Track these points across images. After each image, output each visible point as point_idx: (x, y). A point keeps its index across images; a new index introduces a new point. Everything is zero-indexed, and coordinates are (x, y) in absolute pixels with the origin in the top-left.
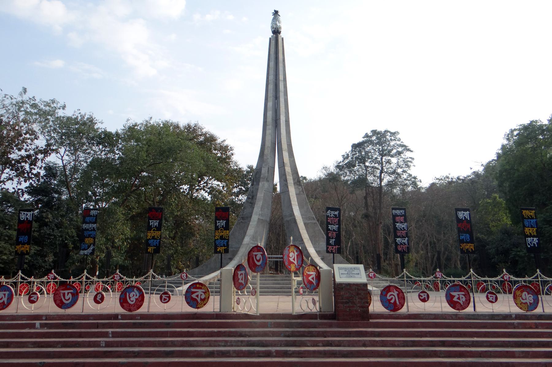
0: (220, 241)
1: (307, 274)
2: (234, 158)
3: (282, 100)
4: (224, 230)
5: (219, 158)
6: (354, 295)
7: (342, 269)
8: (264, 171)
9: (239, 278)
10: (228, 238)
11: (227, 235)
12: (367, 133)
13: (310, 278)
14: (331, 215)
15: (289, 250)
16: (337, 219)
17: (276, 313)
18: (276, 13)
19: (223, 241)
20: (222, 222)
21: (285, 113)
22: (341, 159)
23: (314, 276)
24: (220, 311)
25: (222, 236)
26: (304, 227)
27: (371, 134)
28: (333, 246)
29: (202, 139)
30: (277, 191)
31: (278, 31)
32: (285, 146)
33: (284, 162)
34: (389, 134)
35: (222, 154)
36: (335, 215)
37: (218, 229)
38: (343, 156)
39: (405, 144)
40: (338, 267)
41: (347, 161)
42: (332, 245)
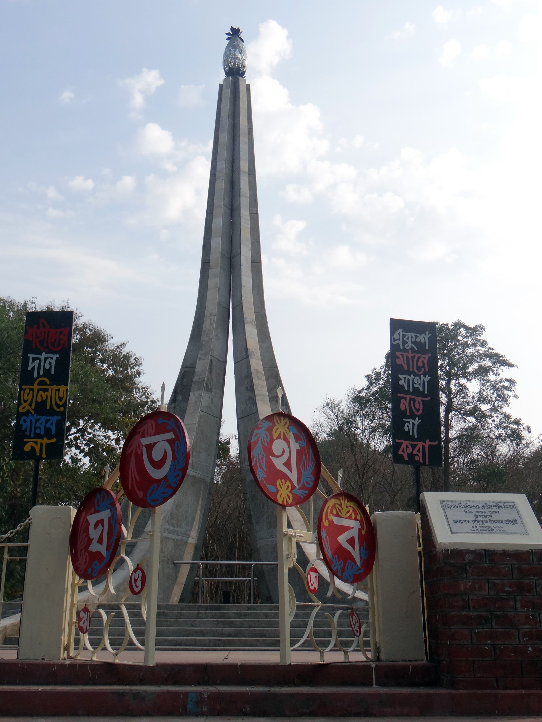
1: (331, 522)
2: (142, 381)
3: (245, 213)
4: (52, 384)
5: (110, 379)
6: (507, 592)
7: (454, 506)
9: (91, 537)
10: (62, 409)
13: (342, 539)
14: (404, 343)
15: (270, 430)
18: (235, 33)
19: (44, 418)
20: (46, 359)
21: (252, 243)
22: (365, 383)
23: (354, 533)
24: (18, 658)
25: (44, 402)
30: (229, 457)
31: (238, 69)
32: (249, 313)
33: (246, 349)
34: (463, 331)
35: (116, 371)
36: (419, 345)
37: (31, 381)
38: (368, 377)
39: (498, 350)
40: (442, 502)
41: (376, 389)
42: (412, 438)
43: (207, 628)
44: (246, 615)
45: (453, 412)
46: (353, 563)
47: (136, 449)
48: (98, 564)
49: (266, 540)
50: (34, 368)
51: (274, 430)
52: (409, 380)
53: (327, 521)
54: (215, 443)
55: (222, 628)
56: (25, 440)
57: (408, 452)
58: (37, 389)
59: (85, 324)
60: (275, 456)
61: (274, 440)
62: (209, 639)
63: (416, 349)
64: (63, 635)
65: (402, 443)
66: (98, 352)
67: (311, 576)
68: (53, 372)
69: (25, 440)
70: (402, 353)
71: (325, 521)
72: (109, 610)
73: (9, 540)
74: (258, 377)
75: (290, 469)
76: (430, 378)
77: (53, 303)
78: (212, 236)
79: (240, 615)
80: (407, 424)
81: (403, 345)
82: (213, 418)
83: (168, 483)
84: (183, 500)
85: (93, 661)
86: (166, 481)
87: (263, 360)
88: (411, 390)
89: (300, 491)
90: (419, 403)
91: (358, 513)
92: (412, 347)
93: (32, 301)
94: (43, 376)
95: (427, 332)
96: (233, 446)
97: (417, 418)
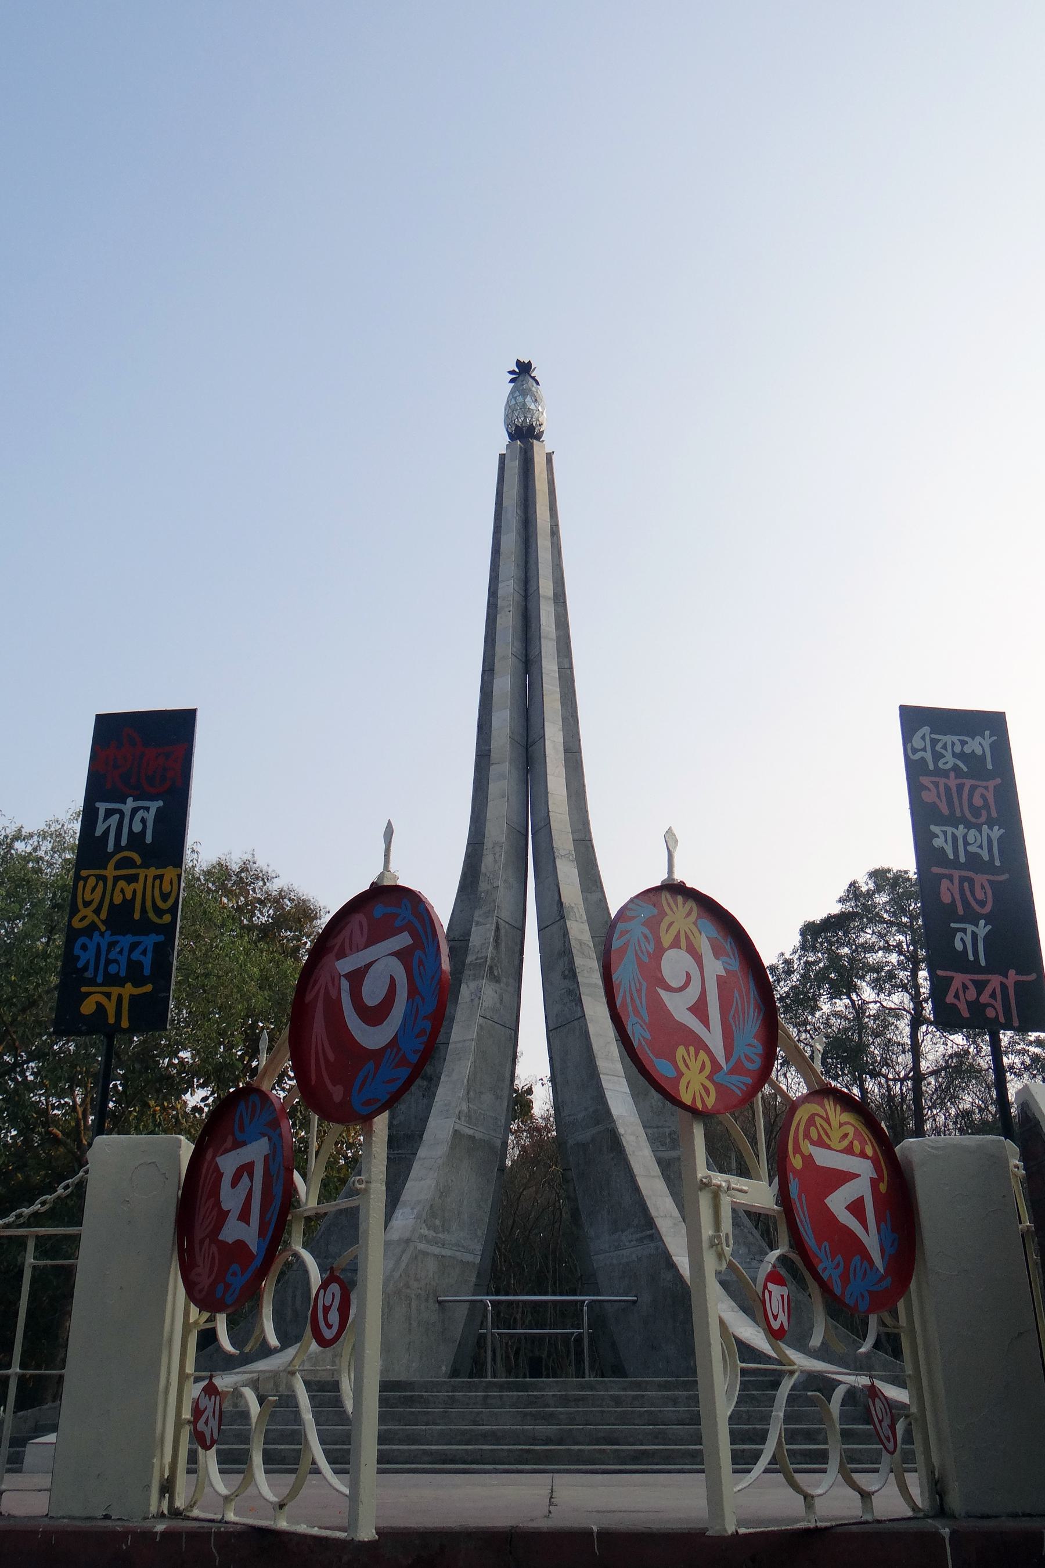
0: (108, 938)
1: (808, 1160)
3: (550, 666)
4: (145, 865)
8: (480, 937)
9: (225, 1207)
10: (167, 918)
11: (165, 897)
12: (855, 882)
13: (837, 1202)
14: (937, 756)
16: (991, 784)
17: (544, 1524)
18: (524, 369)
20: (134, 811)
23: (860, 1188)
25: (128, 905)
26: (656, 1170)
27: (872, 886)
28: (980, 970)
29: (262, 917)
30: (532, 1117)
31: (531, 428)
33: (560, 903)
43: (505, 1427)
44: (578, 1400)
45: (924, 1028)
46: (866, 1264)
47: (327, 989)
48: (239, 1272)
49: (607, 1254)
50: (107, 831)
51: (664, 926)
52: (955, 838)
53: (798, 1156)
54: (506, 1093)
55: (532, 1427)
56: (84, 989)
57: (970, 999)
58: (114, 877)
59: (281, 891)
60: (668, 988)
61: (663, 951)
62: (510, 1450)
63: (965, 769)
64: (158, 1453)
65: (952, 978)
66: (304, 938)
67: (770, 1293)
68: (149, 839)
69: (84, 989)
70: (934, 779)
71: (794, 1156)
72: (317, 1393)
73: (36, 1219)
74: (583, 954)
75: (706, 1022)
76: (1002, 831)
77: (228, 856)
78: (494, 709)
79: (565, 1401)
80: (959, 935)
81: (936, 764)
82: (503, 1028)
83: (402, 1052)
84: (452, 1181)
85: (226, 1522)
86: (395, 1050)
87: (590, 921)
88: (962, 859)
89: (735, 1078)
90: (983, 887)
91: (867, 1139)
92: (955, 765)
93: (192, 848)
94: (128, 848)
95: (987, 733)
96: (537, 1097)
97: (982, 922)
